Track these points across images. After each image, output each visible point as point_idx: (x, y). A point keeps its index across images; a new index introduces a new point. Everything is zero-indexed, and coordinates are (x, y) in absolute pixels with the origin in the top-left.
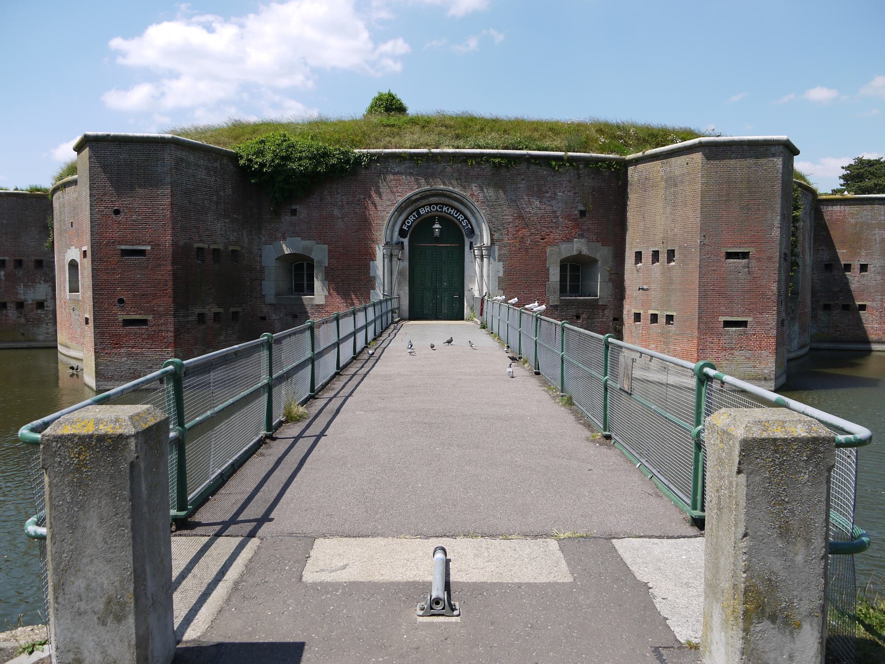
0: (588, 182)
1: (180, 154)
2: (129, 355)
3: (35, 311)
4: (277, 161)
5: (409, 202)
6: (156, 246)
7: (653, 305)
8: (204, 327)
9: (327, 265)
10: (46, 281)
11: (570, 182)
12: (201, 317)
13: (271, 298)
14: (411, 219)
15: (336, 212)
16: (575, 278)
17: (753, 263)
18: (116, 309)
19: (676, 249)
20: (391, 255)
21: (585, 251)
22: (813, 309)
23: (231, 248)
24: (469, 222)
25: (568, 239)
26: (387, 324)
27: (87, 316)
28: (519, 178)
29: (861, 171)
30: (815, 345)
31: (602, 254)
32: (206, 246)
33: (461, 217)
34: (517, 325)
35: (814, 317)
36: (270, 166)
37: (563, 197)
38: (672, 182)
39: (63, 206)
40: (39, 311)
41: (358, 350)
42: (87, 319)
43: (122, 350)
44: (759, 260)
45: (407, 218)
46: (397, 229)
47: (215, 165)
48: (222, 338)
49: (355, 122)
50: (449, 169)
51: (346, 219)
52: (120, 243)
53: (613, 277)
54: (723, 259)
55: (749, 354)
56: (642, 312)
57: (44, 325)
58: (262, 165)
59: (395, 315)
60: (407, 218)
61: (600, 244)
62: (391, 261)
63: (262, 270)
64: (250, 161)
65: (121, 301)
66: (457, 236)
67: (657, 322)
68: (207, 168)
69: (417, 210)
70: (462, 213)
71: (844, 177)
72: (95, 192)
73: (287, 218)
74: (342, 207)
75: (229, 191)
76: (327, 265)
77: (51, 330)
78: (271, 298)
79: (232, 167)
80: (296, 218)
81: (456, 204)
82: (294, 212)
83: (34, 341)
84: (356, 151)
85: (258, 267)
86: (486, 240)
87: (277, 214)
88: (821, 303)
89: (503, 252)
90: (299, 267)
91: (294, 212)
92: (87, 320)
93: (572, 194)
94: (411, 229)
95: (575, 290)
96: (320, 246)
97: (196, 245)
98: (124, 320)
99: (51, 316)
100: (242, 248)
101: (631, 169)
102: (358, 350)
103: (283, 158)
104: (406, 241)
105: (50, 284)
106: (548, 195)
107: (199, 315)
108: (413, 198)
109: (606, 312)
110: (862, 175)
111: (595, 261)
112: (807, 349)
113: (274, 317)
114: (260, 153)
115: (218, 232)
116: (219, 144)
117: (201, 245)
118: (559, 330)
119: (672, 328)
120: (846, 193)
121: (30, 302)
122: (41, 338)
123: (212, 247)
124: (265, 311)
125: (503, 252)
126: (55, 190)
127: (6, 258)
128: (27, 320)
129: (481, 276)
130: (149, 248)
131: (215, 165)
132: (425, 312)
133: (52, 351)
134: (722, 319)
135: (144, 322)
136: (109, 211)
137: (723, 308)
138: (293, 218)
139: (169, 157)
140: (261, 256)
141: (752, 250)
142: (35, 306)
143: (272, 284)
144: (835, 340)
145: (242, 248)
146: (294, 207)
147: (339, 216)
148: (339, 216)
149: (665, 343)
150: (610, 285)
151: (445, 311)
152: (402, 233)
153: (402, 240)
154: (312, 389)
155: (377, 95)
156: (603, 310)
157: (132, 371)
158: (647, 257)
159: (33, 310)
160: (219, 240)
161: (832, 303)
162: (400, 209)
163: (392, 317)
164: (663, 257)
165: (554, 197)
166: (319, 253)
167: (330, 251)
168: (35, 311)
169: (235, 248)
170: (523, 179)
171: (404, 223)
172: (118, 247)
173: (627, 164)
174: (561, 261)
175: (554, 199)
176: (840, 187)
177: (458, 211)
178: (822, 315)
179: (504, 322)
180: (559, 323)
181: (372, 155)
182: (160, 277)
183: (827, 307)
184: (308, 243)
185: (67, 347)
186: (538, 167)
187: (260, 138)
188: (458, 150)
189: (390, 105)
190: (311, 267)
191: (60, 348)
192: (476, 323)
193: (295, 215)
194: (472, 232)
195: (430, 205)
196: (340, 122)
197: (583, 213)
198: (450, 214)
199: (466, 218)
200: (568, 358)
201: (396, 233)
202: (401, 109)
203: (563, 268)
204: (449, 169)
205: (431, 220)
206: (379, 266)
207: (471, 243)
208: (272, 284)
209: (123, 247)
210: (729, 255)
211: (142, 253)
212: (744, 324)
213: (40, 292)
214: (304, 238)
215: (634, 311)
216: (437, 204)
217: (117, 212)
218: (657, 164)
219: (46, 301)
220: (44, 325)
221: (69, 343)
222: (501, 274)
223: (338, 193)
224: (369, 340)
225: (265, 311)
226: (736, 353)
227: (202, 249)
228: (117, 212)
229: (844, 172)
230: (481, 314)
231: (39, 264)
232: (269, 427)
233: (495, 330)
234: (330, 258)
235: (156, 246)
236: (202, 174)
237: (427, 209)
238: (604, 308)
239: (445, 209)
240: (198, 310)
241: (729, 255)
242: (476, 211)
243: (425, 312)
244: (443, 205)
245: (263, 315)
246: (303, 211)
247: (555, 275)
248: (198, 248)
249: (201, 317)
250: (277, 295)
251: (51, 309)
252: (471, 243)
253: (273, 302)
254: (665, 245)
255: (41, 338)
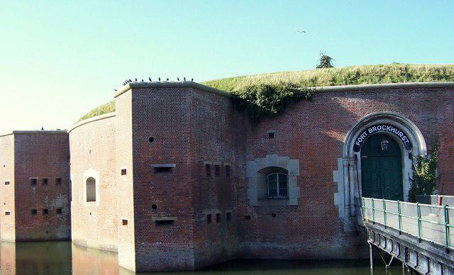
1: (196, 95)
18: (150, 213)
20: (349, 165)
23: (225, 164)
33: (401, 134)
40: (58, 216)
45: (359, 137)
46: (352, 145)
60: (359, 137)
65: (154, 207)
69: (367, 130)
72: (32, 136)
78: (254, 201)
81: (398, 124)
92: (125, 222)
97: (206, 163)
104: (358, 154)
108: (365, 121)
115: (217, 154)
117: (208, 163)
127: (37, 178)
130: (174, 165)
139: (189, 97)
152: (356, 148)
153: (356, 153)
157: (162, 260)
167: (301, 164)
169: (227, 164)
171: (357, 140)
172: (30, 178)
184: (285, 158)
195: (376, 126)
196: (199, 84)
199: (405, 135)
201: (352, 149)
206: (338, 176)
211: (167, 170)
214: (280, 155)
216: (381, 125)
234: (301, 170)
236: (208, 109)
237: (374, 129)
239: (388, 128)
240: (206, 212)
244: (386, 125)
245: (248, 215)
248: (207, 165)
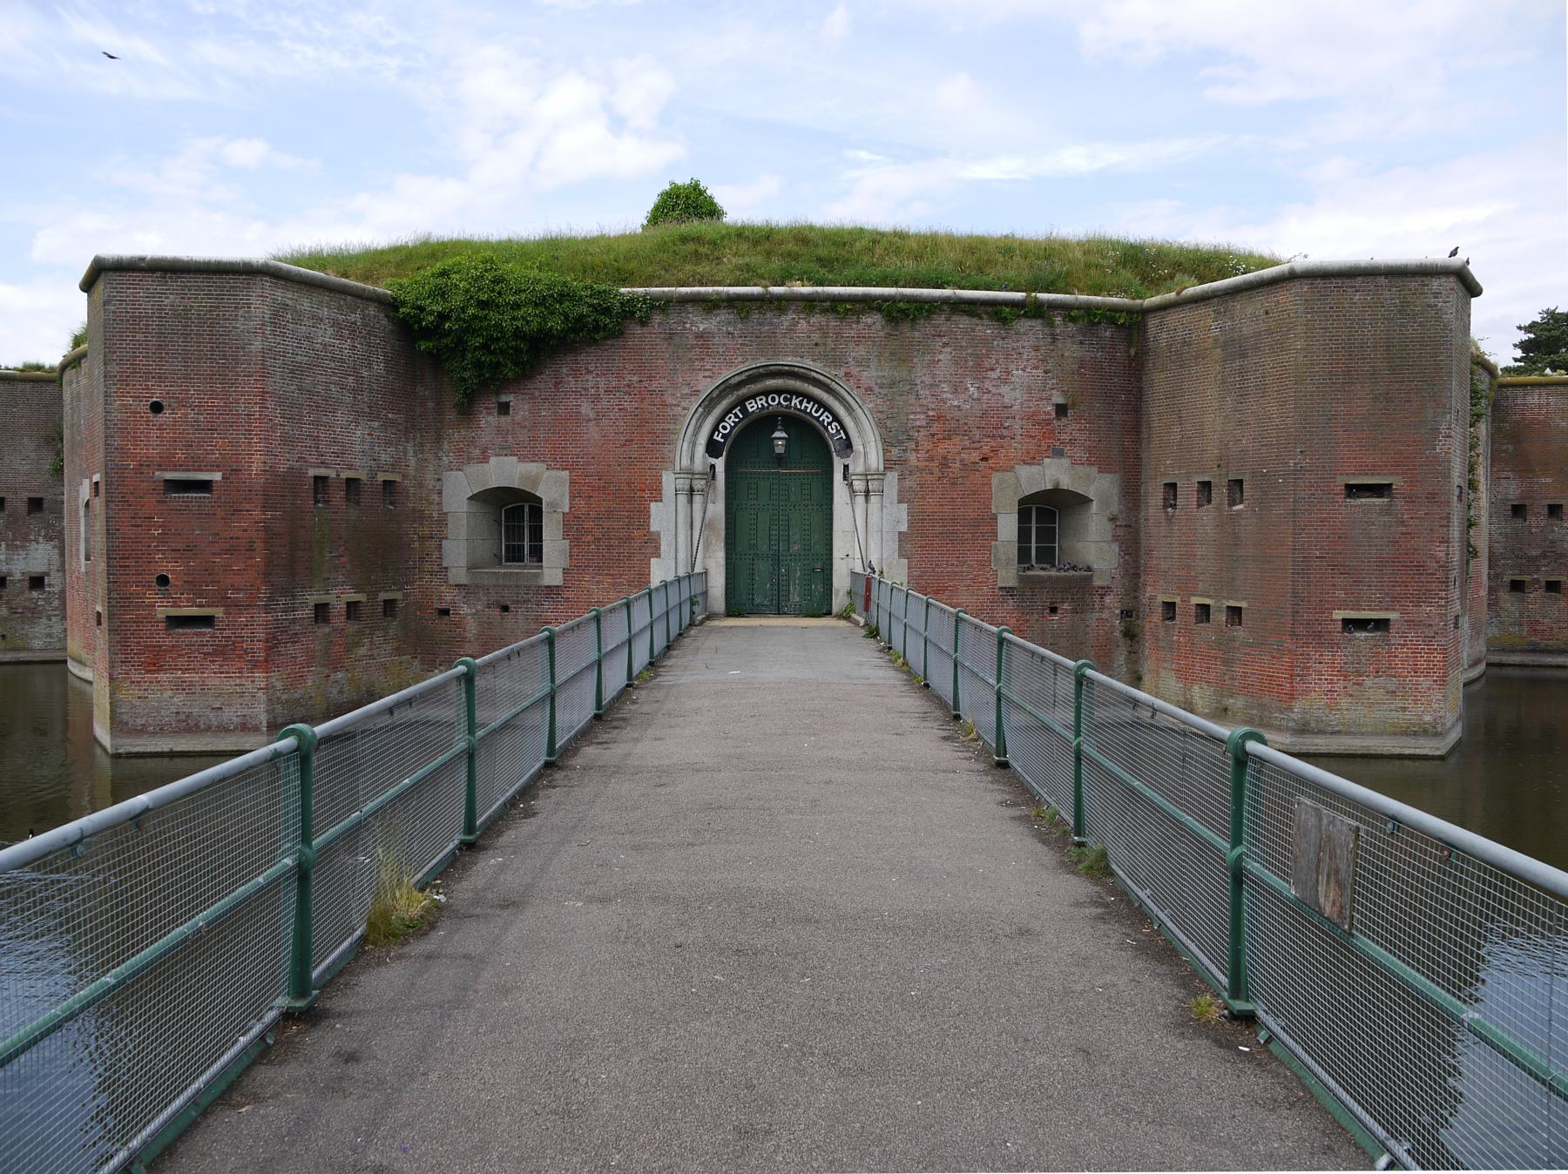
0: (1072, 350)
2: (179, 686)
3: (27, 595)
4: (471, 311)
5: (726, 388)
6: (232, 472)
7: (1201, 586)
8: (327, 630)
9: (567, 510)
10: (49, 538)
11: (1037, 349)
12: (321, 611)
13: (459, 574)
14: (731, 421)
15: (586, 409)
16: (1047, 535)
17: (1399, 503)
18: (151, 596)
19: (1246, 478)
20: (692, 490)
21: (1066, 483)
22: (1491, 590)
23: (381, 477)
24: (843, 427)
25: (1031, 460)
26: (688, 620)
27: (99, 608)
28: (939, 342)
29: (1557, 333)
30: (1496, 658)
31: (1100, 487)
32: (333, 475)
33: (826, 418)
34: (947, 646)
35: (1493, 604)
36: (458, 319)
37: (1022, 378)
38: (1235, 349)
39: (77, 397)
40: (35, 594)
41: (606, 700)
42: (99, 614)
43: (162, 676)
44: (1410, 500)
45: (722, 419)
47: (352, 318)
48: (363, 651)
49: (632, 238)
50: (803, 325)
51: (605, 422)
52: (160, 467)
53: (1120, 532)
54: (1340, 498)
55: (1392, 684)
56: (1177, 600)
57: (44, 620)
58: (443, 317)
59: (697, 609)
60: (722, 419)
61: (1094, 469)
62: (691, 501)
63: (442, 520)
64: (421, 309)
65: (163, 580)
66: (815, 448)
67: (1208, 620)
68: (335, 323)
70: (828, 409)
71: (1523, 346)
73: (488, 421)
74: (596, 399)
75: (379, 368)
76: (567, 510)
77: (57, 629)
78: (459, 574)
79: (385, 322)
80: (508, 419)
82: (504, 409)
83: (24, 649)
84: (622, 290)
85: (435, 514)
86: (875, 460)
87: (466, 410)
88: (1507, 579)
89: (907, 483)
90: (514, 515)
91: (504, 409)
93: (1040, 372)
94: (730, 440)
95: (1047, 556)
96: (554, 473)
97: (312, 472)
98: (169, 618)
99: (56, 603)
100: (404, 476)
101: (1153, 323)
102: (606, 700)
103: (483, 305)
104: (720, 463)
105: (56, 542)
106: (994, 375)
107: (317, 606)
108: (733, 381)
109: (1108, 600)
110: (1555, 338)
111: (1084, 501)
112: (1482, 667)
113: (465, 610)
114: (441, 293)
115: (356, 446)
116: (345, 275)
117: (322, 472)
118: (1067, 686)
119: (1240, 633)
120: (1548, 371)
121: (18, 576)
122: (37, 644)
123: (344, 476)
124: (448, 598)
125: (907, 483)
126: (64, 367)
128: (13, 611)
129: (865, 531)
131: (352, 318)
132: (758, 600)
133: (58, 667)
134: (1339, 615)
135: (208, 621)
136: (144, 407)
137: (1340, 594)
138: (503, 419)
140: (440, 492)
141: (1397, 481)
142: (27, 584)
143: (461, 546)
144: (1534, 650)
145: (404, 476)
146: (504, 398)
147: (592, 415)
148: (592, 415)
149: (1226, 662)
150: (1115, 547)
151: (795, 598)
152: (713, 449)
153: (713, 461)
154: (470, 827)
155: (667, 187)
156: (1102, 596)
158: (1188, 494)
159: (22, 593)
160: (358, 463)
161: (1526, 578)
162: (710, 403)
163: (692, 613)
164: (1220, 494)
165: (1005, 379)
166: (553, 488)
168: (27, 595)
170: (945, 345)
171: (715, 429)
173: (1146, 312)
174: (1021, 502)
175: (1006, 382)
176: (1512, 364)
177: (821, 405)
178: (1507, 600)
179: (918, 633)
180: (1071, 663)
181: (655, 298)
182: (240, 534)
183: (1517, 586)
184: (532, 468)
185: (80, 662)
186: (975, 320)
187: (439, 266)
188: (820, 289)
189: (685, 203)
190: (537, 513)
191: (72, 666)
192: (857, 623)
193: (507, 413)
194: (848, 445)
197: (1061, 410)
198: (804, 411)
199: (836, 418)
200: (1094, 753)
202: (713, 212)
203: (1024, 516)
204: (803, 325)
205: (766, 422)
206: (664, 516)
207: (846, 467)
208: (461, 546)
209: (169, 476)
210: (1353, 490)
211: (205, 486)
212: (1382, 625)
213: (39, 556)
214: (523, 459)
215: (1161, 598)
216: (779, 392)
217: (157, 408)
218: (1205, 314)
219: (48, 574)
220: (44, 620)
221: (84, 656)
222: (904, 528)
223: (589, 372)
224: (636, 669)
225: (448, 598)
226: (1368, 682)
227: (324, 479)
228: (157, 408)
229: (1525, 337)
230: (867, 609)
231: (36, 504)
232: (301, 985)
233: (897, 643)
234: (573, 497)
235: (232, 472)
236: (325, 335)
238: (1106, 590)
239: (795, 401)
240: (314, 598)
241: (1353, 490)
242: (855, 406)
243: (758, 600)
245: (444, 606)
246: (522, 408)
247: (1008, 527)
248: (316, 478)
249: (321, 611)
250: (471, 567)
251: (57, 589)
252: (846, 467)
253: (464, 580)
254: (1224, 471)
255: (37, 644)
